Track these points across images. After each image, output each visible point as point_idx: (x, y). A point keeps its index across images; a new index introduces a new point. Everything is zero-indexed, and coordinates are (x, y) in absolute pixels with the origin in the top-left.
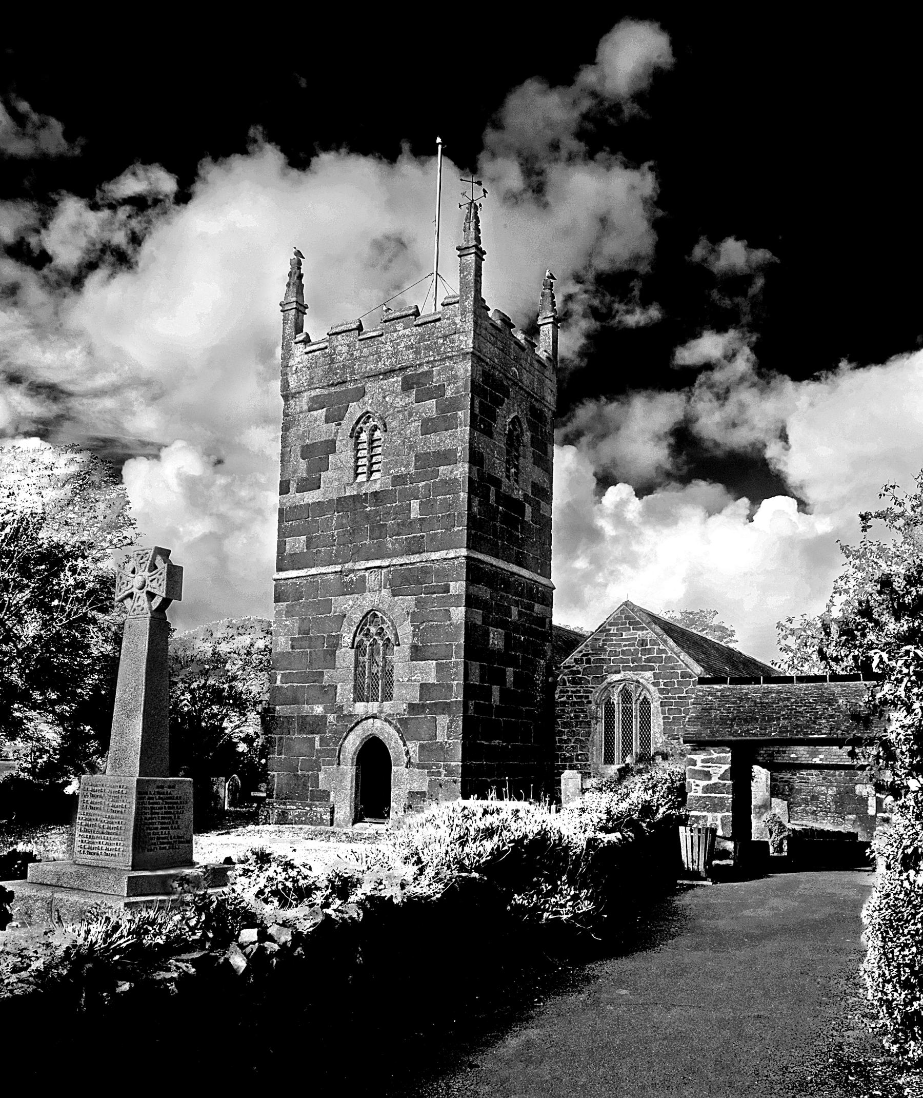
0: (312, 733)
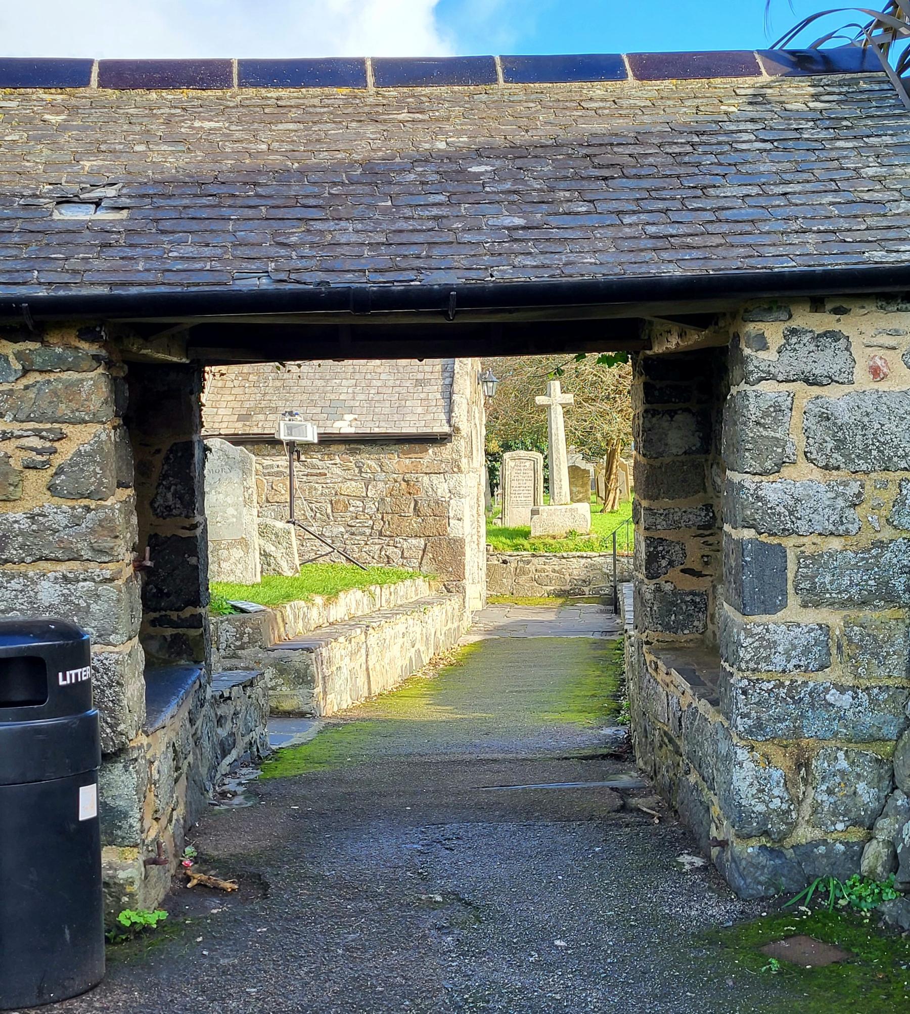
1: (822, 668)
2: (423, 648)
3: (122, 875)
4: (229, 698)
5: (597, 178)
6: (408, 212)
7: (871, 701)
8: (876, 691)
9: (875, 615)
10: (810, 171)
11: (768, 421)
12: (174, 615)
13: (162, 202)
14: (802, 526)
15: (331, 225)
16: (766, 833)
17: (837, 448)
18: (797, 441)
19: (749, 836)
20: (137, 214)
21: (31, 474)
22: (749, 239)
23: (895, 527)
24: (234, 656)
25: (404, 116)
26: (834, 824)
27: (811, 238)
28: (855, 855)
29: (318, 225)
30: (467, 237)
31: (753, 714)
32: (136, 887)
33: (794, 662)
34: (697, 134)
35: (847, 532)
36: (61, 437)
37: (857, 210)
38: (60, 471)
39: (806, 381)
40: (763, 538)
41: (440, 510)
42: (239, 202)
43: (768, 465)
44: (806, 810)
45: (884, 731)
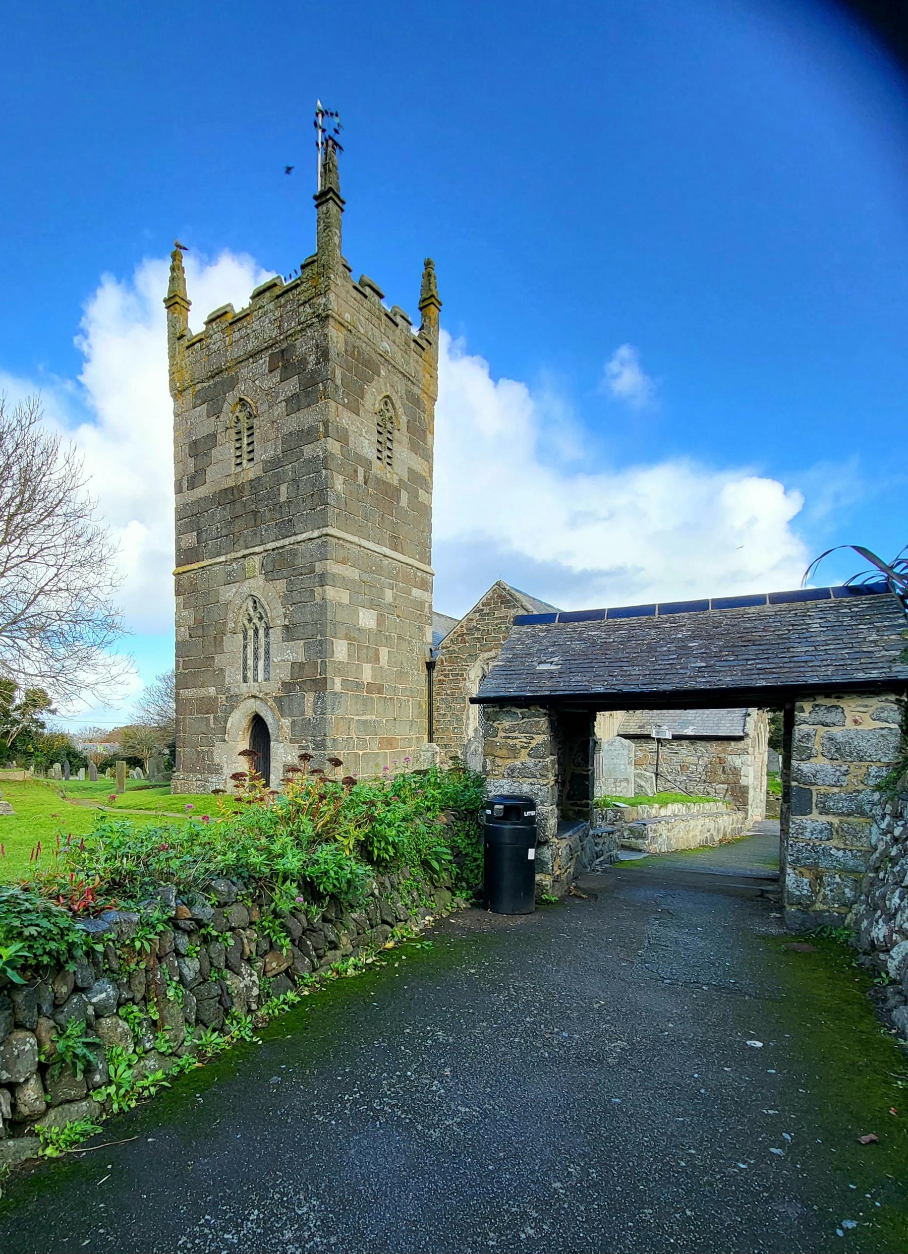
0: (208, 713)
1: (828, 840)
2: (715, 833)
3: (544, 883)
4: (601, 836)
5: (742, 646)
6: (660, 662)
7: (852, 856)
8: (855, 851)
9: (855, 820)
10: (842, 639)
11: (804, 740)
12: (579, 802)
13: (572, 662)
14: (820, 782)
15: (630, 668)
16: (800, 904)
17: (836, 752)
18: (817, 748)
19: (793, 904)
20: (564, 666)
21: (522, 750)
22: (801, 669)
23: (866, 785)
24: (613, 824)
25: (668, 625)
26: (833, 904)
27: (831, 668)
28: (842, 917)
29: (625, 668)
30: (681, 671)
31: (795, 855)
32: (548, 887)
33: (815, 836)
34: (793, 625)
35: (841, 786)
36: (533, 738)
37: (857, 656)
38: (532, 749)
39: (822, 725)
40: (801, 785)
41: (736, 772)
42: (599, 661)
43: (804, 757)
44: (820, 897)
45: (860, 868)
